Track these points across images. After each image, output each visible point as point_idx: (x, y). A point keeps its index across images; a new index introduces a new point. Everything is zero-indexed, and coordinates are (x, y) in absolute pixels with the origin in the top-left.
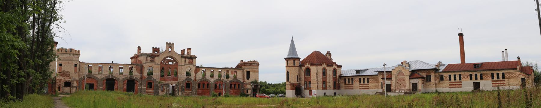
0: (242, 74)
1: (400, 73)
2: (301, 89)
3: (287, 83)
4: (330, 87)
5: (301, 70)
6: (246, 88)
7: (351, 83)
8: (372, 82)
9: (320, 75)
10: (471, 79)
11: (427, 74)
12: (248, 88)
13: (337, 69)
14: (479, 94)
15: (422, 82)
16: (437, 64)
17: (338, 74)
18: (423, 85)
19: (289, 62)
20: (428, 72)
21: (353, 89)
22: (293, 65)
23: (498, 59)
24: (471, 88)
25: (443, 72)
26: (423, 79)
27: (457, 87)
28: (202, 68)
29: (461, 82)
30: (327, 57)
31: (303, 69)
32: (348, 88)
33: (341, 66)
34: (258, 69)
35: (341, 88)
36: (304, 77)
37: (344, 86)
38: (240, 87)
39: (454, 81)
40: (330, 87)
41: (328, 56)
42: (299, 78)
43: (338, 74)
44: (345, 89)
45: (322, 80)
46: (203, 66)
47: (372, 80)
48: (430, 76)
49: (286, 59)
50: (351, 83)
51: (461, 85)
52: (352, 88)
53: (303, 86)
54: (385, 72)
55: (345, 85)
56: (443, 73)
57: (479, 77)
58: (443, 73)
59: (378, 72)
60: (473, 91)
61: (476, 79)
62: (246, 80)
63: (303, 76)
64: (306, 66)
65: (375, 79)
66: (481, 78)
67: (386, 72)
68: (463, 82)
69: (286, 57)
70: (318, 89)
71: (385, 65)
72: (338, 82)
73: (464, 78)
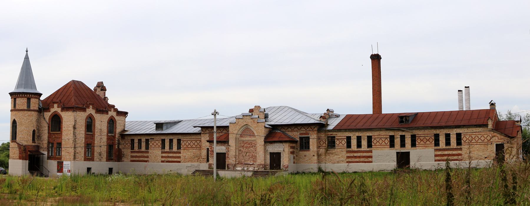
4: (100, 155)
8: (187, 148)
9: (81, 129)
10: (392, 145)
11: (301, 134)
13: (117, 118)
14: (408, 177)
15: (291, 150)
18: (292, 156)
20: (303, 130)
22: (26, 108)
24: (391, 164)
26: (294, 145)
27: (363, 162)
29: (371, 152)
30: (97, 93)
31: (45, 116)
32: (137, 159)
33: (125, 114)
35: (123, 159)
36: (48, 133)
37: (130, 154)
40: (100, 155)
41: (99, 92)
42: (36, 134)
43: (119, 130)
47: (187, 143)
48: (308, 138)
49: (11, 94)
51: (371, 157)
52: (146, 159)
55: (132, 152)
56: (335, 133)
57: (408, 141)
58: (335, 132)
60: (395, 171)
61: (403, 145)
64: (52, 110)
65: (194, 142)
66: (413, 145)
67: (217, 127)
68: (376, 152)
69: (13, 90)
71: (215, 114)
72: (118, 146)
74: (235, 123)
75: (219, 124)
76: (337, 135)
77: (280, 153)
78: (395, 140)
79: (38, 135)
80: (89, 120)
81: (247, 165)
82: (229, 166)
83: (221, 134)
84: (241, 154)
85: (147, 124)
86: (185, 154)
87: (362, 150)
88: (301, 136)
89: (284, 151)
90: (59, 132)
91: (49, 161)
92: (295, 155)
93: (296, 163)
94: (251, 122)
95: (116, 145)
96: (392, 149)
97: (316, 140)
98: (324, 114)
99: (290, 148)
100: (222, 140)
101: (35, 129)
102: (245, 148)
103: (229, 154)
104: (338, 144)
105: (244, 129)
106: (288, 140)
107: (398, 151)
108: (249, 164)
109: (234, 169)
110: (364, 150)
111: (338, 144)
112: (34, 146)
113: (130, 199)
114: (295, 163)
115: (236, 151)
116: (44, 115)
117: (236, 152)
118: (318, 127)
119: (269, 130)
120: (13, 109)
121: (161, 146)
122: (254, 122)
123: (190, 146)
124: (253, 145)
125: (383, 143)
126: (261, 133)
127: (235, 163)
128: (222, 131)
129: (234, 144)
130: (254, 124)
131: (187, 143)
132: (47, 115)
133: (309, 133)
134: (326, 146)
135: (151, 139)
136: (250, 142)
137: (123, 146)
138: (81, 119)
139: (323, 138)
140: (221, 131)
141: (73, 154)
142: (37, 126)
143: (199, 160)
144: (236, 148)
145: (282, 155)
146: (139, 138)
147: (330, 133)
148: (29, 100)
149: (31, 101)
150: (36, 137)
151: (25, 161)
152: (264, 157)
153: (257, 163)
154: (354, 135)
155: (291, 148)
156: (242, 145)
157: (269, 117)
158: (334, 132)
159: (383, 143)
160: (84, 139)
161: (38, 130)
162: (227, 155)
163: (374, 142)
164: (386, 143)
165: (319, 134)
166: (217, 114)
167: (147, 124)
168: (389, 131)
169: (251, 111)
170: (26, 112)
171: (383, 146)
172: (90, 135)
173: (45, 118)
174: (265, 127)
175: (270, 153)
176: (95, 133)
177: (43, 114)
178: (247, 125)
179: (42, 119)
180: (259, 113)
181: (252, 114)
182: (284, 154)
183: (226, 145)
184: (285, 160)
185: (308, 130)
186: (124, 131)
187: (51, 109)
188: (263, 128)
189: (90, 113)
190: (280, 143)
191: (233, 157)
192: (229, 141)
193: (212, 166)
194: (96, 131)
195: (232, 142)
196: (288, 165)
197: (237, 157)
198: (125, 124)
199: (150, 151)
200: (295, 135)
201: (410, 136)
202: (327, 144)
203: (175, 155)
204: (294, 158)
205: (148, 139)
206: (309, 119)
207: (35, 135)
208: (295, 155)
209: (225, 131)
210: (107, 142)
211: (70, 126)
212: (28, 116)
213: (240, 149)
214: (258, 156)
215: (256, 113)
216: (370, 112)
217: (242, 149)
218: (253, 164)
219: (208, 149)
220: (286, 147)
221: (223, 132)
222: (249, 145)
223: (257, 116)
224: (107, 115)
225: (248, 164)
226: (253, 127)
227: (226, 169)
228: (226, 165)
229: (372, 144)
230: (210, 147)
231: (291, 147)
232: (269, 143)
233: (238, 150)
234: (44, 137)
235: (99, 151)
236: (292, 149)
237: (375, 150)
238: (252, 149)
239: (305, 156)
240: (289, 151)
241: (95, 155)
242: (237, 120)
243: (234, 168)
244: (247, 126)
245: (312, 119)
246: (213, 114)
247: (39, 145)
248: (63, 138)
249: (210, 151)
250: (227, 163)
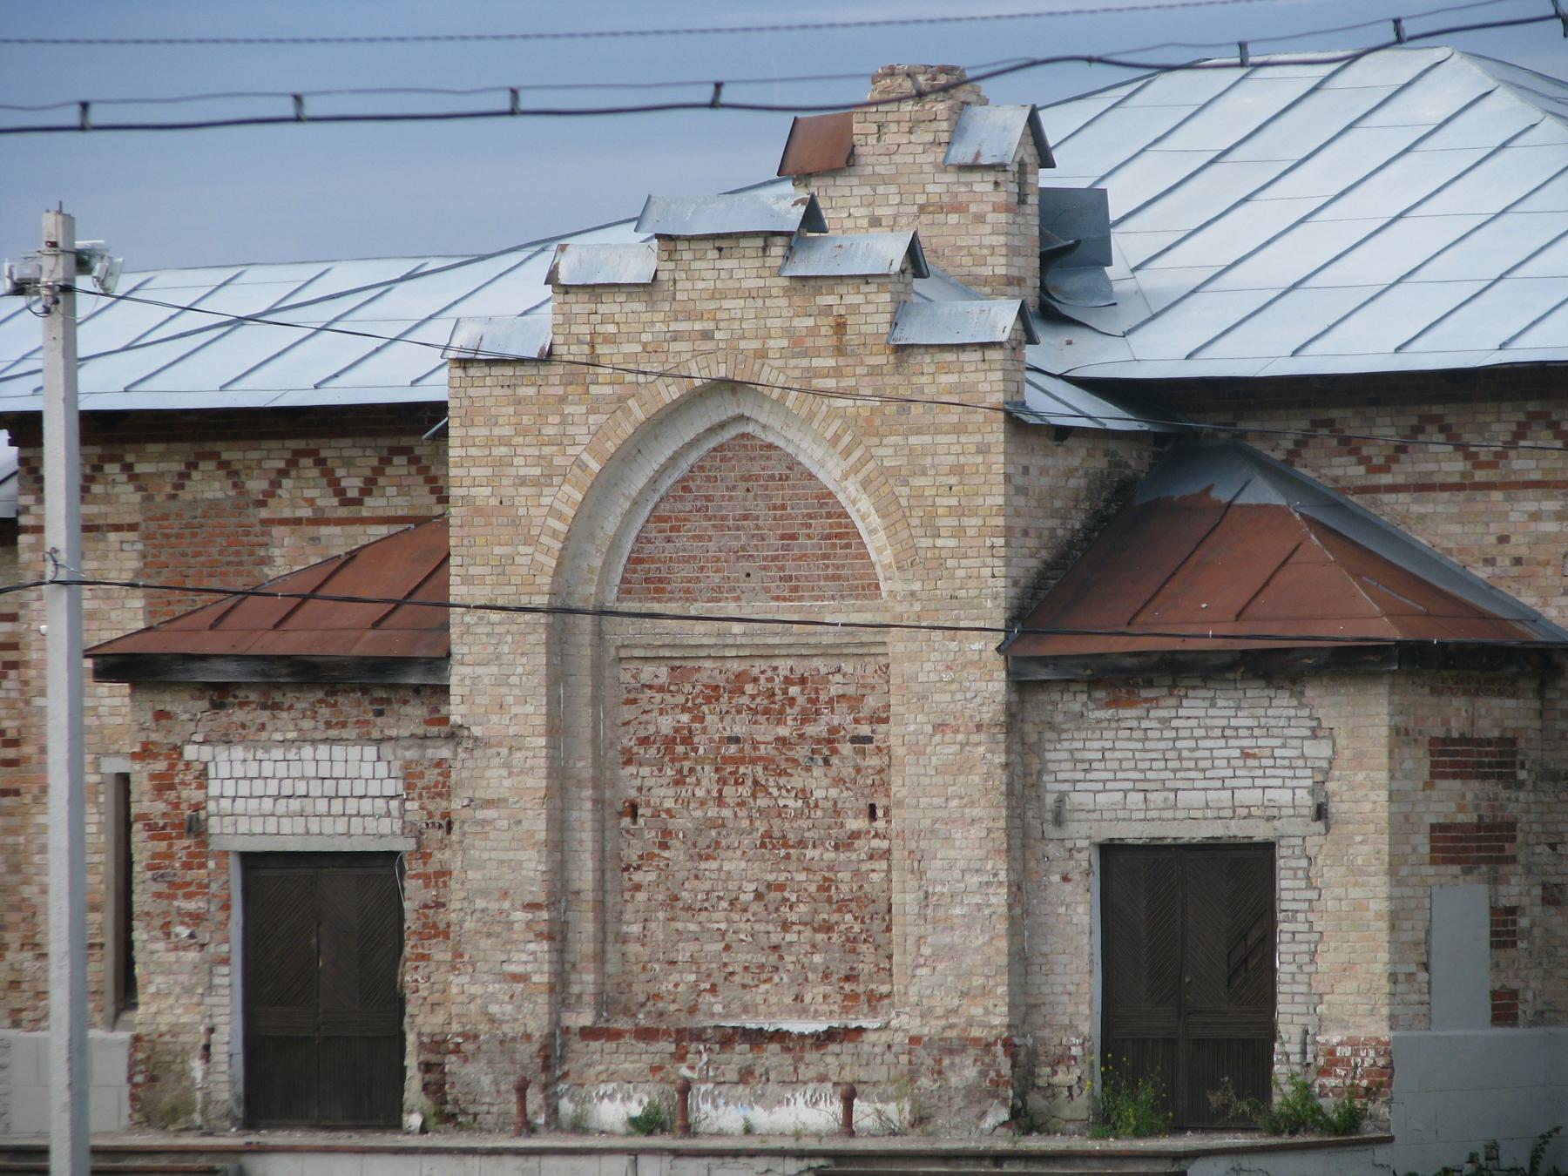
74: (547, 357)
77: (1265, 852)
81: (741, 1053)
82: (452, 1063)
83: (338, 540)
84: (647, 877)
89: (1321, 813)
92: (1516, 889)
93: (1539, 1019)
94: (799, 346)
97: (1284, 906)
99: (1418, 761)
100: (334, 650)
102: (708, 773)
103: (444, 873)
105: (693, 457)
106: (1386, 630)
108: (780, 1036)
109: (528, 1128)
113: (641, 857)
114: (1525, 1010)
115: (559, 826)
117: (558, 845)
119: (1100, 463)
122: (840, 350)
124: (839, 717)
126: (959, 532)
127: (556, 1022)
128: (352, 485)
129: (535, 711)
130: (837, 372)
136: (784, 666)
140: (340, 492)
144: (559, 778)
145: (1288, 885)
152: (1013, 921)
153: (907, 1022)
155: (1437, 773)
156: (666, 724)
157: (1126, 246)
162: (414, 894)
166: (83, 282)
174: (1019, 424)
175: (1110, 851)
178: (729, 386)
180: (939, 187)
181: (813, 219)
182: (1329, 873)
183: (410, 717)
184: (1348, 968)
188: (983, 449)
190: (1256, 693)
191: (520, 916)
192: (441, 661)
193: (184, 1074)
195: (502, 681)
196: (1386, 1050)
197: (585, 926)
200: (1520, 545)
208: (1516, 889)
209: (403, 489)
213: (629, 781)
214: (905, 900)
215: (885, 180)
217: (664, 795)
218: (830, 1036)
219: (124, 779)
220: (1359, 760)
221: (373, 505)
222: (766, 732)
223: (889, 250)
225: (757, 1038)
227: (414, 1120)
228: (411, 1062)
230: (146, 753)
232: (1093, 683)
233: (599, 802)
238: (819, 784)
240: (1400, 827)
242: (579, 306)
243: (535, 1099)
244: (728, 408)
246: (20, 289)
249: (157, 833)
250: (420, 1023)
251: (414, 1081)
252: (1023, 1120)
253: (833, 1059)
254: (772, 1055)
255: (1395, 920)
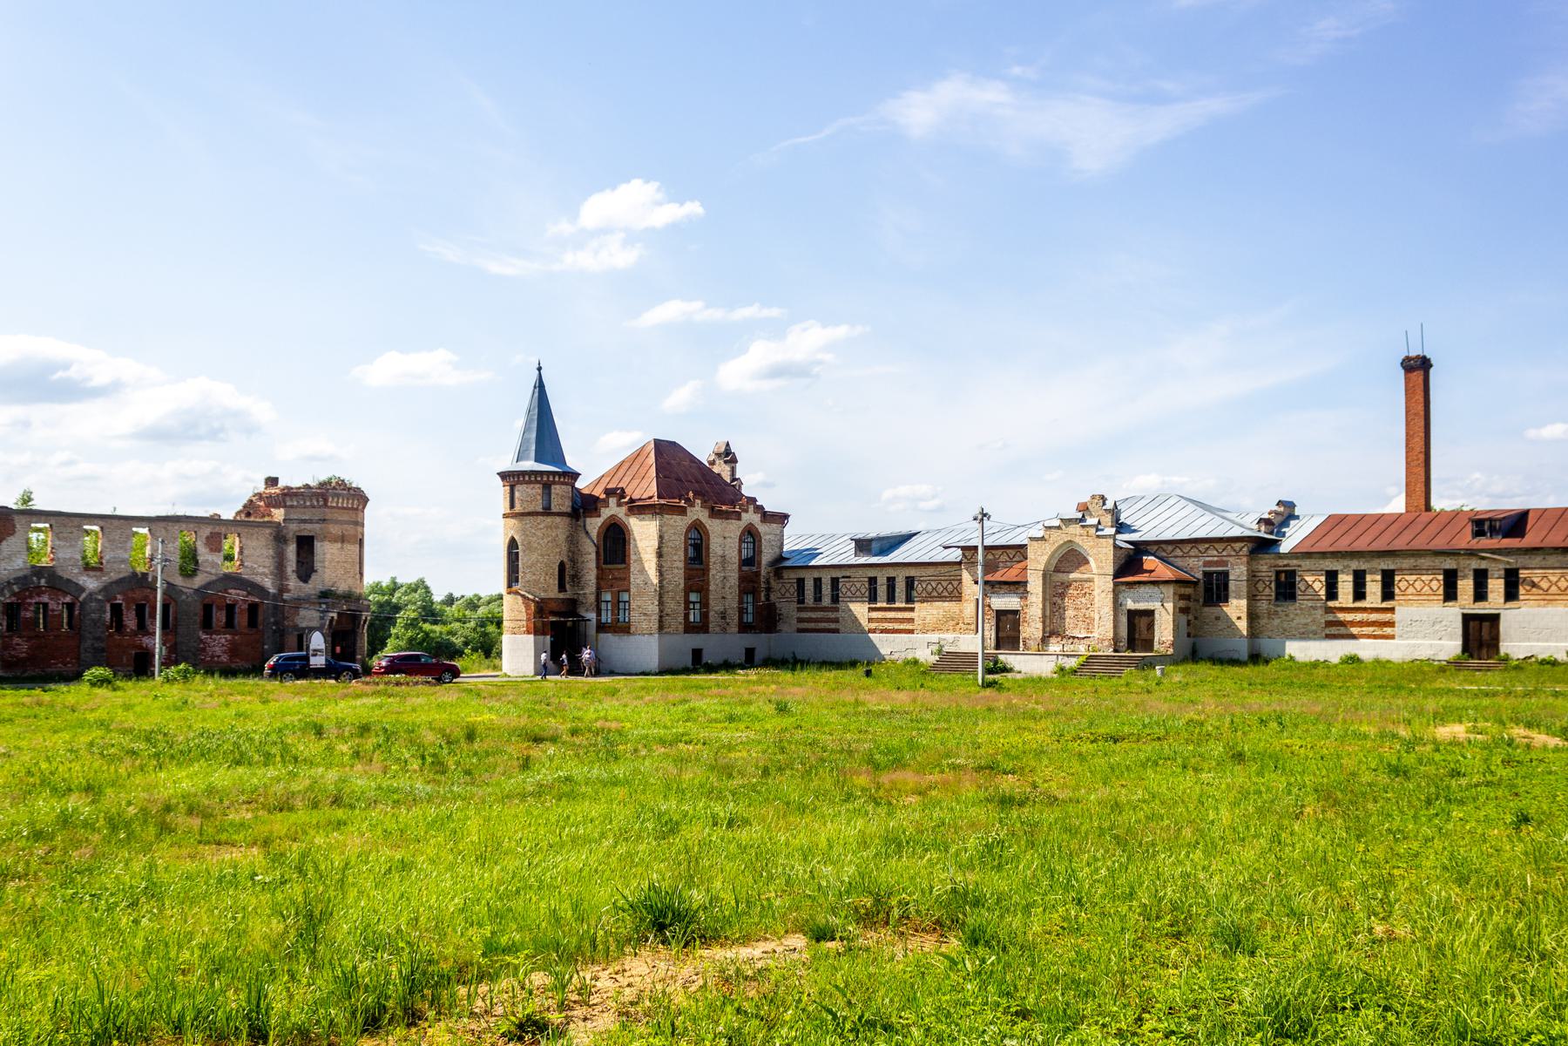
0: (271, 552)
1: (1071, 558)
2: (582, 629)
3: (508, 599)
4: (724, 618)
5: (583, 535)
6: (296, 627)
7: (826, 601)
8: (929, 598)
9: (675, 558)
10: (1450, 594)
11: (1206, 564)
12: (304, 625)
13: (763, 528)
14: (1493, 681)
15: (1182, 604)
16: (1266, 516)
17: (767, 556)
18: (1183, 619)
19: (517, 494)
20: (1213, 554)
21: (836, 631)
22: (540, 509)
23: (109, 512)
24: (1450, 645)
25: (1293, 555)
26: (1188, 591)
27: (1369, 637)
28: (27, 518)
29: (1392, 610)
30: (716, 469)
31: (589, 528)
32: (812, 625)
33: (782, 518)
34: (363, 525)
35: (780, 626)
36: (597, 568)
37: (796, 615)
38: (260, 618)
39: (1352, 605)
40: (724, 618)
41: (721, 469)
42: (569, 572)
43: (767, 556)
44: (800, 631)
45: (682, 586)
46: (39, 504)
47: (930, 587)
48: (1226, 574)
49: (504, 476)
50: (826, 601)
51: (1391, 624)
52: (833, 626)
53: (592, 616)
54: (980, 550)
55: (799, 610)
56: (1295, 562)
57: (1496, 586)
58: (1297, 558)
59: (963, 548)
60: (1456, 664)
61: (1480, 594)
62: (293, 582)
63: (593, 565)
64: (606, 513)
65: (945, 584)
66: (1511, 594)
67: (987, 549)
68: (1404, 611)
69: (509, 464)
70: (661, 628)
71: (983, 516)
72: (767, 597)
73: (1411, 590)
75: (988, 542)
76: (1299, 566)
78: (1459, 582)
79: (572, 573)
80: (694, 535)
85: (836, 543)
86: (923, 614)
87: (1368, 606)
88: (1207, 569)
90: (623, 566)
91: (602, 636)
92: (1191, 617)
95: (763, 594)
96: (1450, 604)
98: (1270, 513)
99: (1177, 597)
101: (565, 560)
104: (1303, 588)
107: (1466, 611)
110: (1372, 606)
111: (1303, 588)
112: (563, 600)
115: (1044, 606)
116: (585, 526)
118: (1250, 545)
120: (508, 511)
121: (867, 594)
123: (935, 594)
124: (1087, 590)
125: (1426, 588)
131: (930, 587)
132: (594, 524)
133: (1227, 561)
134: (1273, 594)
135: (843, 577)
137: (779, 595)
138: (675, 534)
139: (1264, 574)
141: (657, 617)
142: (570, 551)
143: (958, 627)
146: (816, 575)
147: (1281, 562)
148: (547, 487)
149: (553, 491)
150: (567, 579)
151: (541, 637)
154: (1345, 568)
158: (1291, 558)
159: (1426, 588)
160: (682, 581)
161: (573, 561)
163: (1401, 584)
164: (1435, 588)
165: (1254, 563)
167: (836, 543)
168: (1442, 559)
169: (1084, 508)
170: (540, 518)
171: (1425, 597)
172: (697, 569)
173: (587, 532)
176: (708, 565)
177: (585, 522)
179: (583, 535)
185: (1224, 553)
186: (781, 558)
187: (603, 510)
189: (695, 517)
194: (712, 560)
198: (782, 543)
199: (841, 605)
201: (1503, 572)
202: (1273, 588)
203: (900, 615)
204: (1189, 623)
205: (838, 578)
206: (1228, 525)
207: (567, 574)
208: (1191, 617)
210: (739, 586)
211: (648, 549)
212: (547, 527)
216: (1398, 505)
224: (738, 522)
225: (1074, 638)
226: (1086, 544)
229: (1393, 592)
231: (1180, 595)
234: (588, 578)
235: (719, 608)
236: (1184, 602)
237: (1400, 605)
238: (1083, 600)
239: (1217, 618)
241: (711, 619)
245: (1236, 527)
246: (975, 519)
247: (575, 597)
248: (632, 580)
251: (1021, 643)
252: (1115, 651)
253: (1085, 641)
254: (1076, 640)
255: (1174, 621)
